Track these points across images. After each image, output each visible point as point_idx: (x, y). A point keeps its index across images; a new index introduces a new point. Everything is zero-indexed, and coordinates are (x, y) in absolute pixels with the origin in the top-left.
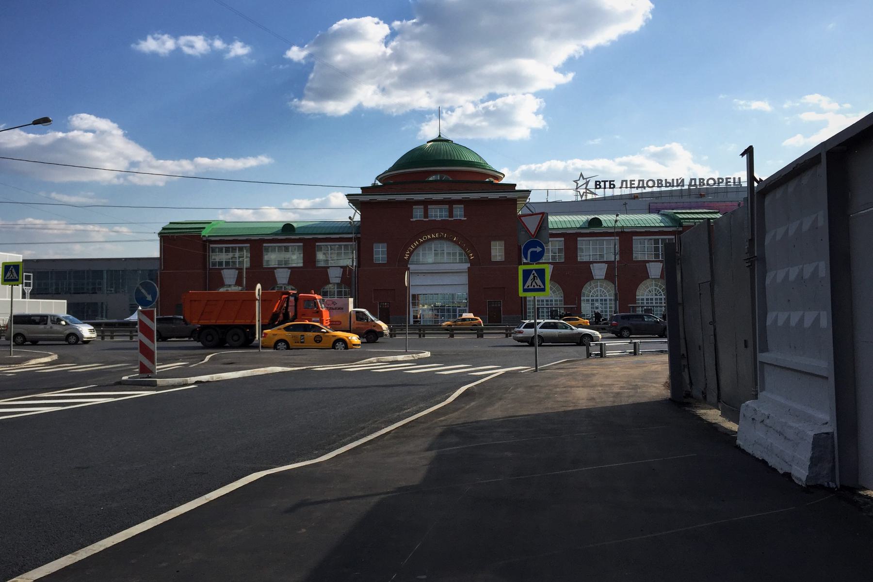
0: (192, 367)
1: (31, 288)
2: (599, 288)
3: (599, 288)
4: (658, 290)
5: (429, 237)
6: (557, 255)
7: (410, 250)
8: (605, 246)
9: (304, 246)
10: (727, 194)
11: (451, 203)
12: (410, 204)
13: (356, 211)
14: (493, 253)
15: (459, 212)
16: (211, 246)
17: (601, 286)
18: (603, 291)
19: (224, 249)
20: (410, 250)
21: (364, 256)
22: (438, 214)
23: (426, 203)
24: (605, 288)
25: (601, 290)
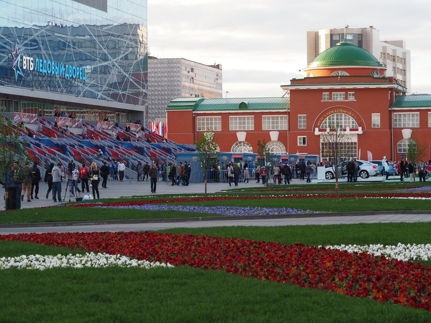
0: (168, 260)
1: (398, 143)
2: (275, 146)
3: (275, 146)
4: (239, 150)
5: (333, 112)
6: (331, 121)
7: (321, 120)
8: (279, 120)
9: (222, 118)
10: (330, 95)
11: (346, 90)
12: (321, 91)
13: (36, 80)
14: (379, 118)
15: (352, 99)
16: (394, 113)
17: (276, 145)
18: (278, 148)
19: (205, 119)
20: (321, 120)
21: (292, 123)
22: (339, 97)
23: (331, 91)
24: (279, 146)
25: (276, 147)
